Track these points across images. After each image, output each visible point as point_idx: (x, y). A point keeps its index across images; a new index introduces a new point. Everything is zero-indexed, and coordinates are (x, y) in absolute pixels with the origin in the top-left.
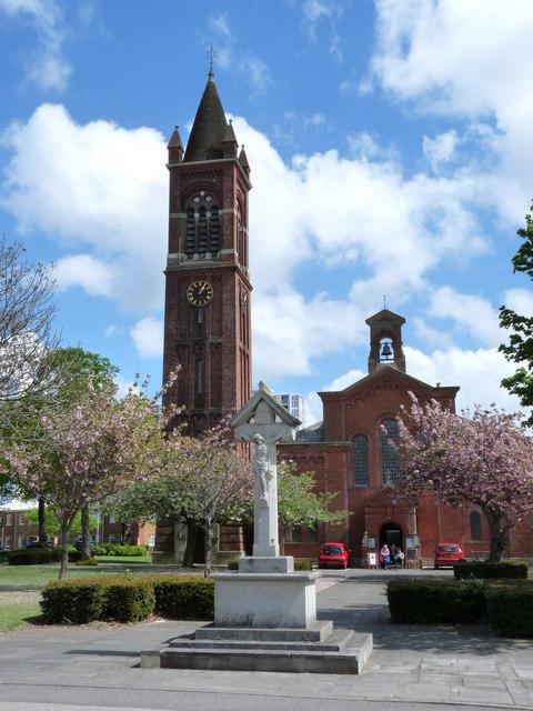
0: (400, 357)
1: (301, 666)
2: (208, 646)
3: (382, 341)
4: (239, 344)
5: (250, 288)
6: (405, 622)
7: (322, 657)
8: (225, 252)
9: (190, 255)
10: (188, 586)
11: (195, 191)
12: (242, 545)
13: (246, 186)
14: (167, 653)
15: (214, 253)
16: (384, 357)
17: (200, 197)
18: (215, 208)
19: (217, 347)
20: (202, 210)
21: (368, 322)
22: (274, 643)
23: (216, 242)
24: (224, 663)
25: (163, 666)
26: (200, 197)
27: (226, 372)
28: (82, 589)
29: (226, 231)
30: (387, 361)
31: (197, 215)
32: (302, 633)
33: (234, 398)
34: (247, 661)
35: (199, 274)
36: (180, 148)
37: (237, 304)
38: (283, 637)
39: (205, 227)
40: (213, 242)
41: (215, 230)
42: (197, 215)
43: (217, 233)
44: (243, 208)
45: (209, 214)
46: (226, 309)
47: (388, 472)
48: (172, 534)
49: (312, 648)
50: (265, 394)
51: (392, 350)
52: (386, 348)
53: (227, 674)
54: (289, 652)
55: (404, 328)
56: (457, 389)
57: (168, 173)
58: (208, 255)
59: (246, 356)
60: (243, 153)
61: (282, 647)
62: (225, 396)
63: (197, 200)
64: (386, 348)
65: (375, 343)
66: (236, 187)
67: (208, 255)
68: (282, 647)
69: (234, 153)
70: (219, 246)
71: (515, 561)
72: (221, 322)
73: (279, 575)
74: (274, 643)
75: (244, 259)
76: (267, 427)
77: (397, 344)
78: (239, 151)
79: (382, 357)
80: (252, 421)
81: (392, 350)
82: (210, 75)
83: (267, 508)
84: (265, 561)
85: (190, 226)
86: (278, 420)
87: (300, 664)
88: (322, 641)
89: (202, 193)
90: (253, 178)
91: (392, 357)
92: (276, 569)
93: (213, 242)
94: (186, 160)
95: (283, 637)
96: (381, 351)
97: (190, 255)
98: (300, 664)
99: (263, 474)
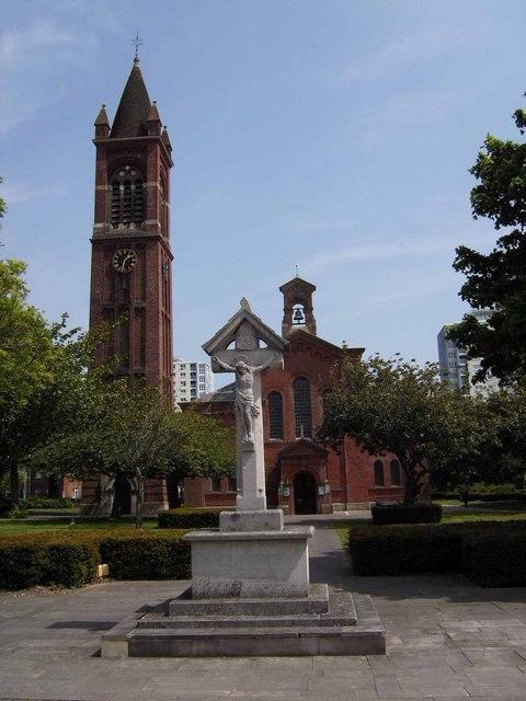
0: (311, 321)
1: (313, 649)
2: (185, 624)
3: (294, 307)
4: (161, 308)
5: (172, 258)
6: (374, 573)
7: (338, 636)
8: (148, 222)
9: (115, 225)
10: (138, 543)
11: (121, 166)
12: (165, 497)
13: (168, 164)
14: (137, 637)
15: (138, 224)
16: (296, 322)
17: (125, 170)
18: (139, 182)
19: (141, 312)
20: (127, 183)
21: (206, 348)
22: (272, 618)
23: (140, 214)
24: (212, 647)
25: (132, 654)
26: (125, 170)
27: (149, 335)
28: (16, 551)
29: (150, 204)
30: (299, 326)
31: (122, 188)
32: (306, 604)
33: (157, 359)
34: (244, 644)
35: (124, 242)
36: (107, 125)
37: (160, 271)
38: (281, 609)
39: (130, 200)
40: (137, 214)
41: (140, 202)
42: (122, 188)
43: (141, 210)
44: (165, 183)
45: (133, 187)
46: (150, 276)
47: (302, 427)
48: (99, 487)
49: (321, 624)
50: (249, 313)
51: (303, 316)
52: (298, 313)
53: (219, 663)
54: (295, 630)
55: (314, 295)
56: (364, 350)
57: (95, 148)
58: (132, 227)
59: (168, 321)
60: (165, 134)
61: (283, 623)
62: (148, 356)
63: (122, 174)
64: (298, 313)
65: (288, 310)
66: (159, 163)
67: (132, 227)
68: (283, 623)
69: (158, 131)
70: (144, 217)
71: (206, 508)
72: (145, 286)
73: (272, 533)
74: (272, 618)
75: (165, 229)
76: (251, 354)
77: (308, 309)
78: (162, 129)
79: (294, 322)
80: (232, 346)
81: (303, 316)
82: (136, 60)
83: (253, 451)
84: (253, 516)
85: (116, 198)
86: (263, 345)
87: (312, 645)
88: (331, 614)
89: (127, 168)
90: (174, 156)
91: (303, 321)
92: (267, 526)
93: (137, 214)
94: (111, 137)
95: (281, 609)
96: (294, 316)
97: (115, 225)
98: (312, 645)
99: (248, 410)
